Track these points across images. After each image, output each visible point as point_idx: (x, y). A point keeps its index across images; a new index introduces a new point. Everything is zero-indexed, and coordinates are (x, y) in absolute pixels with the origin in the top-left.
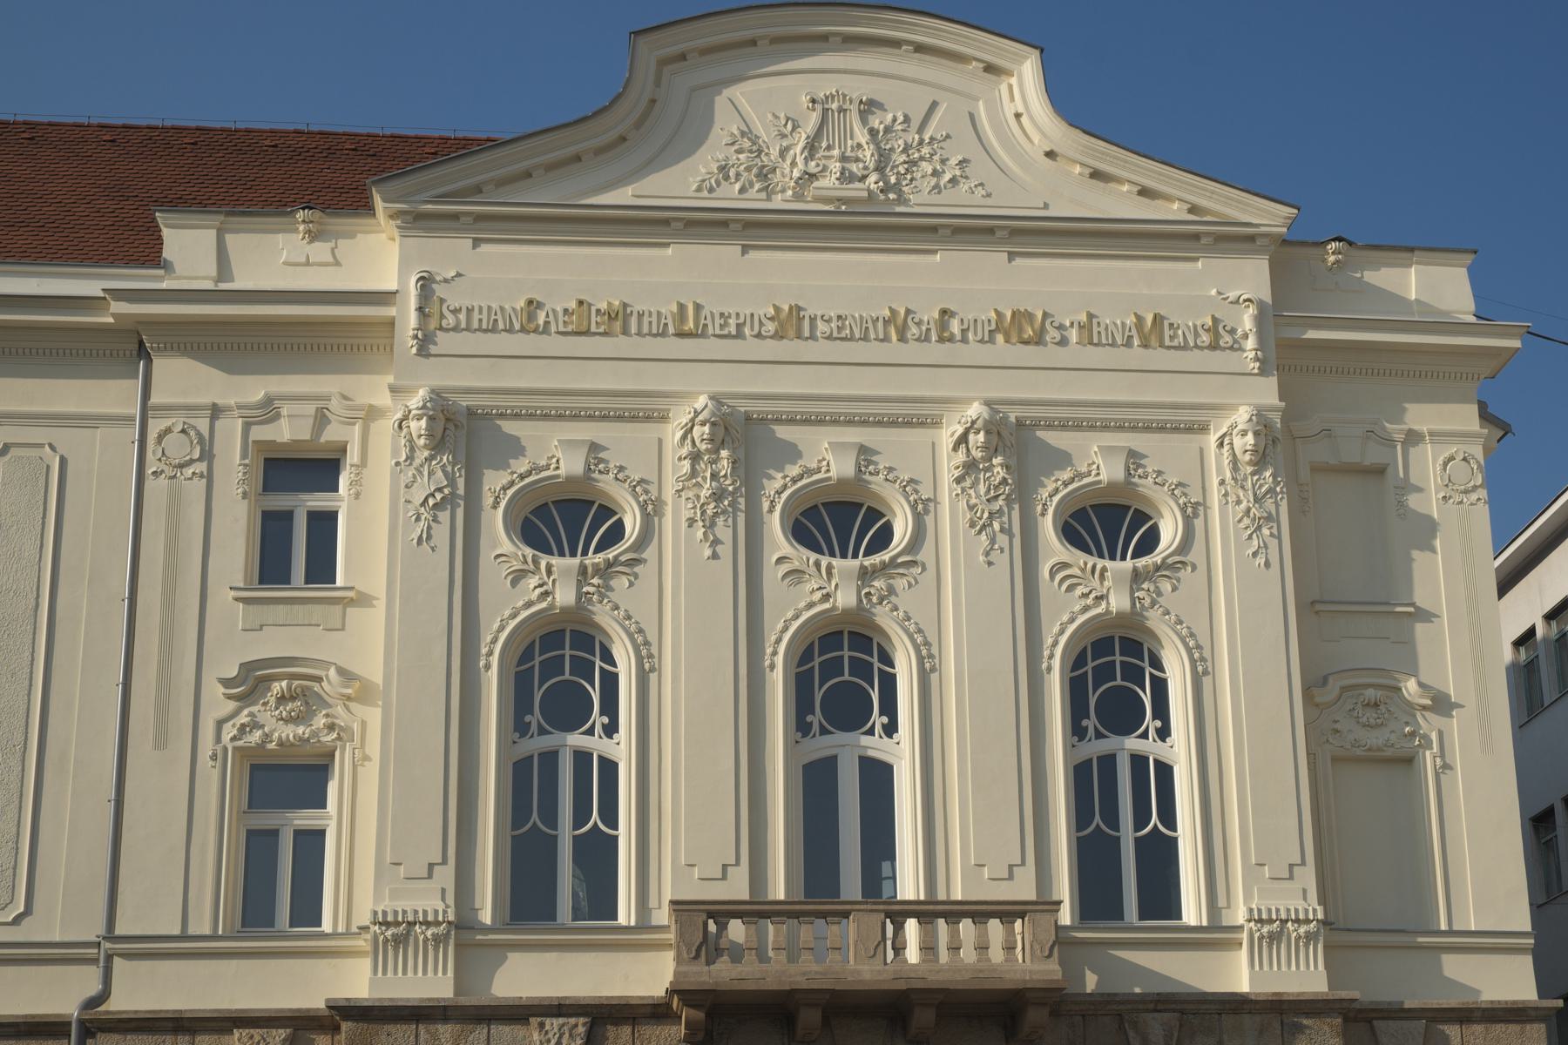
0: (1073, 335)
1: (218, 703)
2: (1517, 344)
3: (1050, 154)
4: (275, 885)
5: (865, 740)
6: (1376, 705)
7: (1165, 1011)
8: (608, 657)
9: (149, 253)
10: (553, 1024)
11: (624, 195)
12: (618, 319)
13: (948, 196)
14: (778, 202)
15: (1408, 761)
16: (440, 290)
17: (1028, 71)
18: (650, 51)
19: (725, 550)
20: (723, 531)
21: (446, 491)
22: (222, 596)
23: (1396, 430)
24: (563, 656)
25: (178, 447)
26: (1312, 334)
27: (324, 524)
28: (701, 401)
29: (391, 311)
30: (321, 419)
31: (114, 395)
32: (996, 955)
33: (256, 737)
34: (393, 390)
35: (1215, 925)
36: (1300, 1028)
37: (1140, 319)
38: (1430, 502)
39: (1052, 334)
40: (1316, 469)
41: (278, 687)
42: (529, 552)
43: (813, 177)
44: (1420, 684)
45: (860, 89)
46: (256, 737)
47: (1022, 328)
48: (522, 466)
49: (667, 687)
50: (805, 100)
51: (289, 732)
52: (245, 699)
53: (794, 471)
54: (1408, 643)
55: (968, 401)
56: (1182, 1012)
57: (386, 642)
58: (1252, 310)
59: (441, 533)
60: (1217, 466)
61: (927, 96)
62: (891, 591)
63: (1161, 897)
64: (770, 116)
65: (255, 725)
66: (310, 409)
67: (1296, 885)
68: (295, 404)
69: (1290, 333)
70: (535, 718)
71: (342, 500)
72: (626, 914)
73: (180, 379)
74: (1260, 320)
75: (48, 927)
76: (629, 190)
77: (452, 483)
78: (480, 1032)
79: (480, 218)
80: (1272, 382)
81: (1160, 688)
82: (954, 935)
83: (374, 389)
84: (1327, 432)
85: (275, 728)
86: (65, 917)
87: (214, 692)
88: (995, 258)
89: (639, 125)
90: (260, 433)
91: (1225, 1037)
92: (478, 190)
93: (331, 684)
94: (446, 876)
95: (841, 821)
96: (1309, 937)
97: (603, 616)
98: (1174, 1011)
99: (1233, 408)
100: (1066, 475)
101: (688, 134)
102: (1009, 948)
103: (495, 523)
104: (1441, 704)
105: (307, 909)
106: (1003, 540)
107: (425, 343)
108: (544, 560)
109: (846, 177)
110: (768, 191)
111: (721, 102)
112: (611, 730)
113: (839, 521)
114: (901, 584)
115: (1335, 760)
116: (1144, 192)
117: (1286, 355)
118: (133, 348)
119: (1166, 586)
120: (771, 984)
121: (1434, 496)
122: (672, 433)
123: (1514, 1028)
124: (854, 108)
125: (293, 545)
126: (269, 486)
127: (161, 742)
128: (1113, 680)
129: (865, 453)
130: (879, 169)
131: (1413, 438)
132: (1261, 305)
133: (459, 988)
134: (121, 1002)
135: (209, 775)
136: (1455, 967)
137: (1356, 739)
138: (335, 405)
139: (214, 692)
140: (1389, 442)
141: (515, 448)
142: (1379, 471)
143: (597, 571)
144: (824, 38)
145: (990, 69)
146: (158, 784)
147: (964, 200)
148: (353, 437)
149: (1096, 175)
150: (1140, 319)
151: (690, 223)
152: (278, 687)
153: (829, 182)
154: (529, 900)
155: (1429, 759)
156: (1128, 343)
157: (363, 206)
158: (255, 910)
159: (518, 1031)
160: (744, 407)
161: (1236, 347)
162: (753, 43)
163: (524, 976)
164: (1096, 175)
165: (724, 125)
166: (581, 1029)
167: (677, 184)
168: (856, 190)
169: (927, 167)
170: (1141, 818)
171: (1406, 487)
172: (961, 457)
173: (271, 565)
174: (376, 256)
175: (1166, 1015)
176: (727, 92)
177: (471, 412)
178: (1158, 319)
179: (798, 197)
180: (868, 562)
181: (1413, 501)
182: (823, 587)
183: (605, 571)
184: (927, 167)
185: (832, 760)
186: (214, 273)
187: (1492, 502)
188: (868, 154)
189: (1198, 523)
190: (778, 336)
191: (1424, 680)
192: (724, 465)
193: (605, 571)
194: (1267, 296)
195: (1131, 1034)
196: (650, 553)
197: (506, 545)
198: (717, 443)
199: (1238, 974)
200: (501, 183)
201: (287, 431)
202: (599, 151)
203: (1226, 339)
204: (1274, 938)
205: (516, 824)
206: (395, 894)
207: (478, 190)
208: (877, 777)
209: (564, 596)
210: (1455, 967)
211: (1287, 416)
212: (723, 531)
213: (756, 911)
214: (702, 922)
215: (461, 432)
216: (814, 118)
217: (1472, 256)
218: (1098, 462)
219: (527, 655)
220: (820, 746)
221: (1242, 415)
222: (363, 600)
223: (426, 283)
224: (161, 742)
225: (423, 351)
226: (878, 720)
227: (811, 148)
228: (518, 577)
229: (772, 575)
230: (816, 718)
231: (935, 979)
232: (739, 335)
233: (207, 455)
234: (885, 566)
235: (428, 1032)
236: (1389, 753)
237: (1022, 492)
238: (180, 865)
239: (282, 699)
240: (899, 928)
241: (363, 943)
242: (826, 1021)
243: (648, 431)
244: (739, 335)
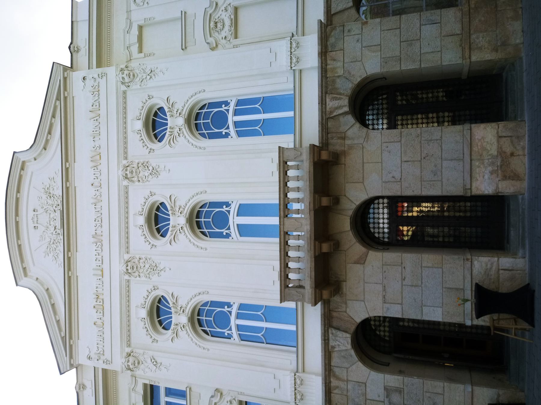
6: (216, 23)
7: (326, 100)
10: (332, 343)
21: (380, 98)
24: (206, 320)
40: (140, 51)
56: (326, 93)
82: (292, 167)
91: (336, 75)
98: (325, 97)
115: (236, 37)
166: (334, 331)
175: (328, 100)
195: (335, 114)
205: (260, 134)
231: (307, 200)
235: (335, 389)
236: (233, 17)
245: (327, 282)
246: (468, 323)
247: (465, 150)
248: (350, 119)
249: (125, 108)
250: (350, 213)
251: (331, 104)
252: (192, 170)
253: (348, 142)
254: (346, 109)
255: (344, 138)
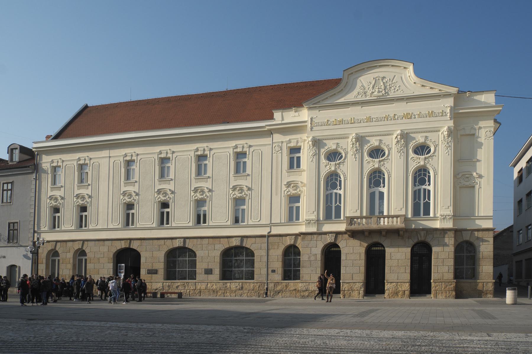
0: (417, 116)
1: (284, 188)
2: (501, 108)
3: (415, 83)
4: (293, 215)
5: (380, 189)
8: (429, 173)
9: (271, 118)
11: (342, 100)
12: (341, 122)
13: (397, 93)
14: (368, 98)
15: (474, 187)
16: (314, 120)
17: (411, 67)
18: (346, 74)
19: (357, 159)
20: (357, 156)
22: (284, 172)
23: (477, 127)
25: (277, 149)
26: (461, 111)
27: (299, 158)
28: (354, 135)
29: (306, 124)
30: (297, 142)
31: (267, 141)
32: (395, 223)
33: (289, 193)
34: (307, 137)
35: (435, 216)
36: (447, 233)
37: (429, 112)
38: (482, 140)
39: (413, 116)
40: (461, 135)
41: (292, 185)
42: (328, 162)
43: (373, 92)
44: (477, 173)
45: (382, 75)
46: (289, 193)
47: (408, 116)
48: (326, 148)
49: (348, 183)
50: (372, 79)
51: (294, 192)
52: (233, 191)
53: (369, 145)
54: (475, 166)
55: (398, 130)
57: (307, 178)
58: (449, 108)
59: (314, 160)
60: (441, 137)
61: (393, 74)
62: (384, 164)
63: (427, 212)
64: (366, 82)
65: (289, 191)
66: (296, 141)
67: (449, 210)
68: (293, 139)
69: (456, 111)
70: (329, 188)
71: (301, 155)
72: (432, 215)
73: (277, 137)
74: (451, 110)
75: (263, 222)
76: (343, 99)
77: (316, 152)
78: (320, 236)
79: (320, 107)
80: (452, 121)
81: (429, 177)
82: (397, 220)
83: (304, 136)
84: (464, 129)
85: (292, 192)
86: (265, 221)
87: (283, 186)
88: (359, 108)
89: (345, 87)
90: (289, 145)
92: (319, 102)
93: (300, 185)
94: (316, 213)
95: (375, 201)
96: (450, 218)
97: (339, 171)
99: (445, 127)
100: (414, 142)
101: (352, 87)
102: (397, 222)
103: (322, 157)
104: (480, 176)
105: (298, 218)
106: (403, 154)
107: (312, 129)
108: (330, 163)
109: (379, 92)
110: (366, 96)
111: (358, 81)
112: (429, 185)
113: (334, 156)
114: (385, 163)
115: (460, 187)
116: (431, 88)
117: (456, 116)
118: (270, 133)
119: (430, 160)
120: (360, 229)
121: (483, 138)
122: (350, 140)
123: (487, 232)
124: (381, 79)
125: (294, 163)
126: (291, 153)
127: (276, 194)
128: (421, 176)
129: (380, 140)
130: (385, 90)
131: (480, 128)
132: (451, 107)
133: (317, 230)
134: (273, 233)
135: (283, 198)
136: (478, 222)
137: (463, 183)
138: (299, 140)
139: (283, 186)
140: (475, 129)
141: (325, 145)
142: (474, 135)
143: (338, 164)
144: (376, 66)
145: (405, 68)
146: (276, 200)
147: (399, 94)
148: (302, 144)
149: (423, 86)
150: (429, 112)
151: (353, 104)
152: (292, 185)
153: (376, 93)
154: (328, 217)
155: (477, 187)
156: (426, 117)
157: (302, 106)
158: (290, 219)
159: (325, 236)
160: (361, 135)
161: (446, 115)
162: (364, 69)
163: (327, 228)
164: (423, 86)
165: (359, 84)
167: (350, 97)
168: (381, 94)
169: (393, 88)
170: (336, 203)
171: (478, 137)
172: (396, 140)
173: (291, 166)
174: (303, 115)
176: (359, 79)
177: (319, 140)
178: (432, 112)
179: (371, 97)
180: (380, 159)
181: (479, 140)
182: (375, 164)
183: (339, 164)
184: (393, 88)
185: (374, 192)
186: (281, 119)
187: (494, 139)
188: (383, 87)
189: (437, 148)
190: (366, 122)
191: (477, 172)
192: (358, 145)
193: (339, 164)
194: (452, 105)
196: (346, 160)
197: (324, 161)
198: (356, 141)
199: (437, 225)
200: (323, 100)
201: (292, 145)
202: (338, 92)
203: (444, 114)
204: (444, 219)
205: (414, 201)
206: (308, 216)
207: (319, 102)
208: (381, 194)
209: (333, 169)
210: (478, 222)
211: (454, 127)
212: (357, 156)
213: (361, 217)
214: (351, 220)
215: (317, 143)
216: (374, 81)
217: (495, 92)
218: (420, 139)
219: (416, 173)
220: (372, 190)
221: (445, 129)
222: (304, 171)
223: (312, 119)
224: (276, 194)
225: (311, 130)
226: (382, 185)
227: (373, 87)
228: (326, 166)
229: (365, 162)
230: (372, 185)
231: (385, 227)
232: (360, 122)
233: (281, 149)
234: (430, 156)
237: (406, 145)
238: (280, 213)
239: (293, 187)
240: (380, 219)
241: (304, 223)
242: (386, 233)
243: (346, 140)
244: (360, 122)
245: (354, 234)
246: (341, 281)
247: (338, 91)
248: (416, 241)
249: (432, 132)
250: (379, 241)
251: (422, 233)
252: (397, 170)
253: (407, 240)
254: (420, 239)
255: (408, 238)
